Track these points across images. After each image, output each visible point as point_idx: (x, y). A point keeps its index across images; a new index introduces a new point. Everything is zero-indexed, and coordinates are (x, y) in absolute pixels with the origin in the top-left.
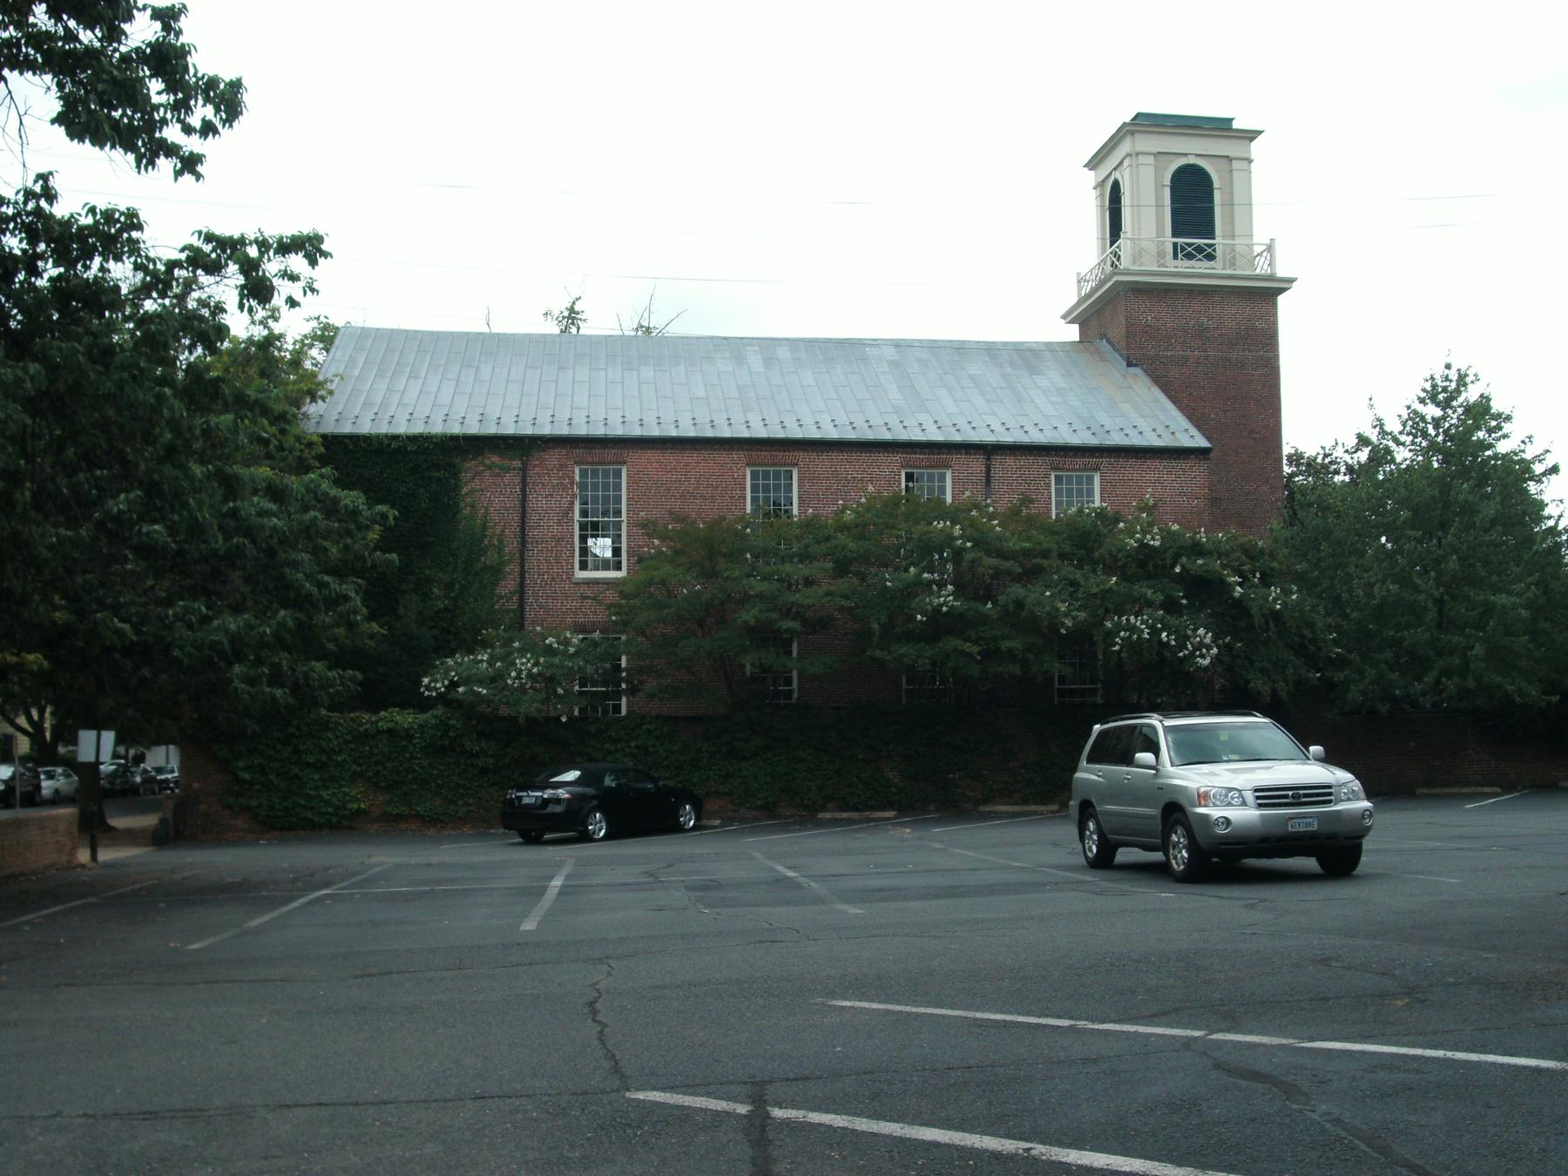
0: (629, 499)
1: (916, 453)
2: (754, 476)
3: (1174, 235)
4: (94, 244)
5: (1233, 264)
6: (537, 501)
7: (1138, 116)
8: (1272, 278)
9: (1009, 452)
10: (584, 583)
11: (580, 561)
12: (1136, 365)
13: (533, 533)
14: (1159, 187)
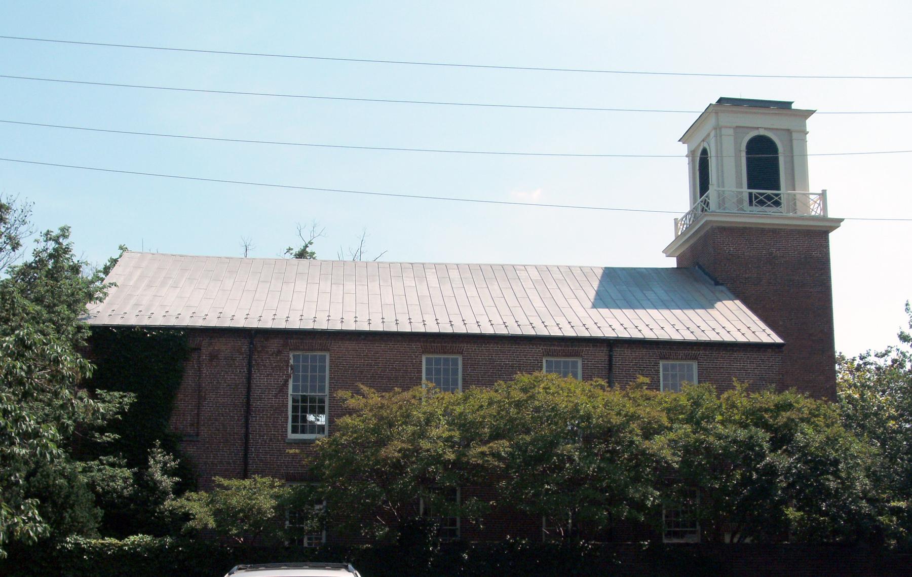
0: (331, 378)
1: (554, 345)
2: (429, 361)
3: (749, 187)
4: (612, 447)
5: (795, 210)
6: (260, 380)
7: (721, 101)
8: (824, 218)
9: (627, 346)
10: (295, 444)
11: (292, 426)
12: (722, 284)
13: (255, 404)
14: (738, 151)
